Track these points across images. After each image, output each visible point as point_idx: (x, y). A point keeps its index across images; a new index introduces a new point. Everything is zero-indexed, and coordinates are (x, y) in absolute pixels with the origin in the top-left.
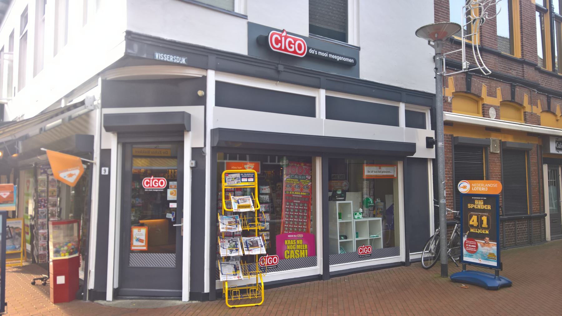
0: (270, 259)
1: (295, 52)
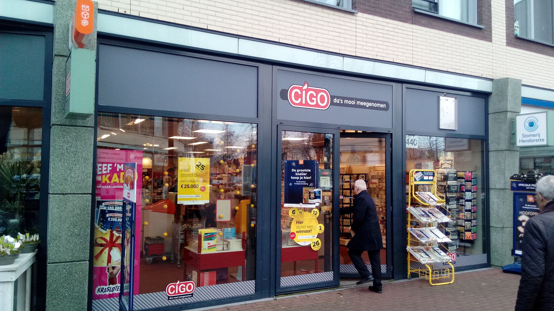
0: (182, 287)
1: (317, 105)
